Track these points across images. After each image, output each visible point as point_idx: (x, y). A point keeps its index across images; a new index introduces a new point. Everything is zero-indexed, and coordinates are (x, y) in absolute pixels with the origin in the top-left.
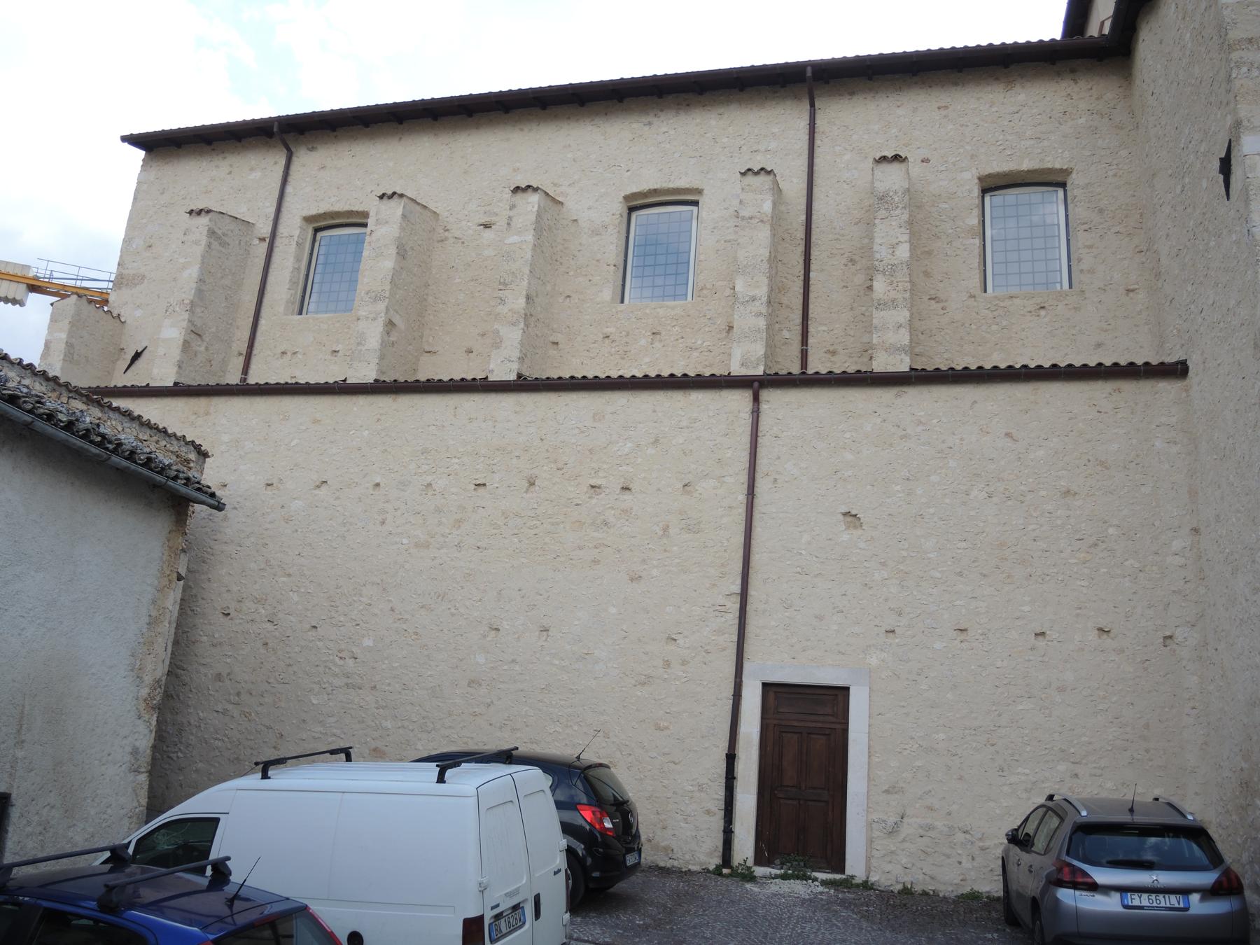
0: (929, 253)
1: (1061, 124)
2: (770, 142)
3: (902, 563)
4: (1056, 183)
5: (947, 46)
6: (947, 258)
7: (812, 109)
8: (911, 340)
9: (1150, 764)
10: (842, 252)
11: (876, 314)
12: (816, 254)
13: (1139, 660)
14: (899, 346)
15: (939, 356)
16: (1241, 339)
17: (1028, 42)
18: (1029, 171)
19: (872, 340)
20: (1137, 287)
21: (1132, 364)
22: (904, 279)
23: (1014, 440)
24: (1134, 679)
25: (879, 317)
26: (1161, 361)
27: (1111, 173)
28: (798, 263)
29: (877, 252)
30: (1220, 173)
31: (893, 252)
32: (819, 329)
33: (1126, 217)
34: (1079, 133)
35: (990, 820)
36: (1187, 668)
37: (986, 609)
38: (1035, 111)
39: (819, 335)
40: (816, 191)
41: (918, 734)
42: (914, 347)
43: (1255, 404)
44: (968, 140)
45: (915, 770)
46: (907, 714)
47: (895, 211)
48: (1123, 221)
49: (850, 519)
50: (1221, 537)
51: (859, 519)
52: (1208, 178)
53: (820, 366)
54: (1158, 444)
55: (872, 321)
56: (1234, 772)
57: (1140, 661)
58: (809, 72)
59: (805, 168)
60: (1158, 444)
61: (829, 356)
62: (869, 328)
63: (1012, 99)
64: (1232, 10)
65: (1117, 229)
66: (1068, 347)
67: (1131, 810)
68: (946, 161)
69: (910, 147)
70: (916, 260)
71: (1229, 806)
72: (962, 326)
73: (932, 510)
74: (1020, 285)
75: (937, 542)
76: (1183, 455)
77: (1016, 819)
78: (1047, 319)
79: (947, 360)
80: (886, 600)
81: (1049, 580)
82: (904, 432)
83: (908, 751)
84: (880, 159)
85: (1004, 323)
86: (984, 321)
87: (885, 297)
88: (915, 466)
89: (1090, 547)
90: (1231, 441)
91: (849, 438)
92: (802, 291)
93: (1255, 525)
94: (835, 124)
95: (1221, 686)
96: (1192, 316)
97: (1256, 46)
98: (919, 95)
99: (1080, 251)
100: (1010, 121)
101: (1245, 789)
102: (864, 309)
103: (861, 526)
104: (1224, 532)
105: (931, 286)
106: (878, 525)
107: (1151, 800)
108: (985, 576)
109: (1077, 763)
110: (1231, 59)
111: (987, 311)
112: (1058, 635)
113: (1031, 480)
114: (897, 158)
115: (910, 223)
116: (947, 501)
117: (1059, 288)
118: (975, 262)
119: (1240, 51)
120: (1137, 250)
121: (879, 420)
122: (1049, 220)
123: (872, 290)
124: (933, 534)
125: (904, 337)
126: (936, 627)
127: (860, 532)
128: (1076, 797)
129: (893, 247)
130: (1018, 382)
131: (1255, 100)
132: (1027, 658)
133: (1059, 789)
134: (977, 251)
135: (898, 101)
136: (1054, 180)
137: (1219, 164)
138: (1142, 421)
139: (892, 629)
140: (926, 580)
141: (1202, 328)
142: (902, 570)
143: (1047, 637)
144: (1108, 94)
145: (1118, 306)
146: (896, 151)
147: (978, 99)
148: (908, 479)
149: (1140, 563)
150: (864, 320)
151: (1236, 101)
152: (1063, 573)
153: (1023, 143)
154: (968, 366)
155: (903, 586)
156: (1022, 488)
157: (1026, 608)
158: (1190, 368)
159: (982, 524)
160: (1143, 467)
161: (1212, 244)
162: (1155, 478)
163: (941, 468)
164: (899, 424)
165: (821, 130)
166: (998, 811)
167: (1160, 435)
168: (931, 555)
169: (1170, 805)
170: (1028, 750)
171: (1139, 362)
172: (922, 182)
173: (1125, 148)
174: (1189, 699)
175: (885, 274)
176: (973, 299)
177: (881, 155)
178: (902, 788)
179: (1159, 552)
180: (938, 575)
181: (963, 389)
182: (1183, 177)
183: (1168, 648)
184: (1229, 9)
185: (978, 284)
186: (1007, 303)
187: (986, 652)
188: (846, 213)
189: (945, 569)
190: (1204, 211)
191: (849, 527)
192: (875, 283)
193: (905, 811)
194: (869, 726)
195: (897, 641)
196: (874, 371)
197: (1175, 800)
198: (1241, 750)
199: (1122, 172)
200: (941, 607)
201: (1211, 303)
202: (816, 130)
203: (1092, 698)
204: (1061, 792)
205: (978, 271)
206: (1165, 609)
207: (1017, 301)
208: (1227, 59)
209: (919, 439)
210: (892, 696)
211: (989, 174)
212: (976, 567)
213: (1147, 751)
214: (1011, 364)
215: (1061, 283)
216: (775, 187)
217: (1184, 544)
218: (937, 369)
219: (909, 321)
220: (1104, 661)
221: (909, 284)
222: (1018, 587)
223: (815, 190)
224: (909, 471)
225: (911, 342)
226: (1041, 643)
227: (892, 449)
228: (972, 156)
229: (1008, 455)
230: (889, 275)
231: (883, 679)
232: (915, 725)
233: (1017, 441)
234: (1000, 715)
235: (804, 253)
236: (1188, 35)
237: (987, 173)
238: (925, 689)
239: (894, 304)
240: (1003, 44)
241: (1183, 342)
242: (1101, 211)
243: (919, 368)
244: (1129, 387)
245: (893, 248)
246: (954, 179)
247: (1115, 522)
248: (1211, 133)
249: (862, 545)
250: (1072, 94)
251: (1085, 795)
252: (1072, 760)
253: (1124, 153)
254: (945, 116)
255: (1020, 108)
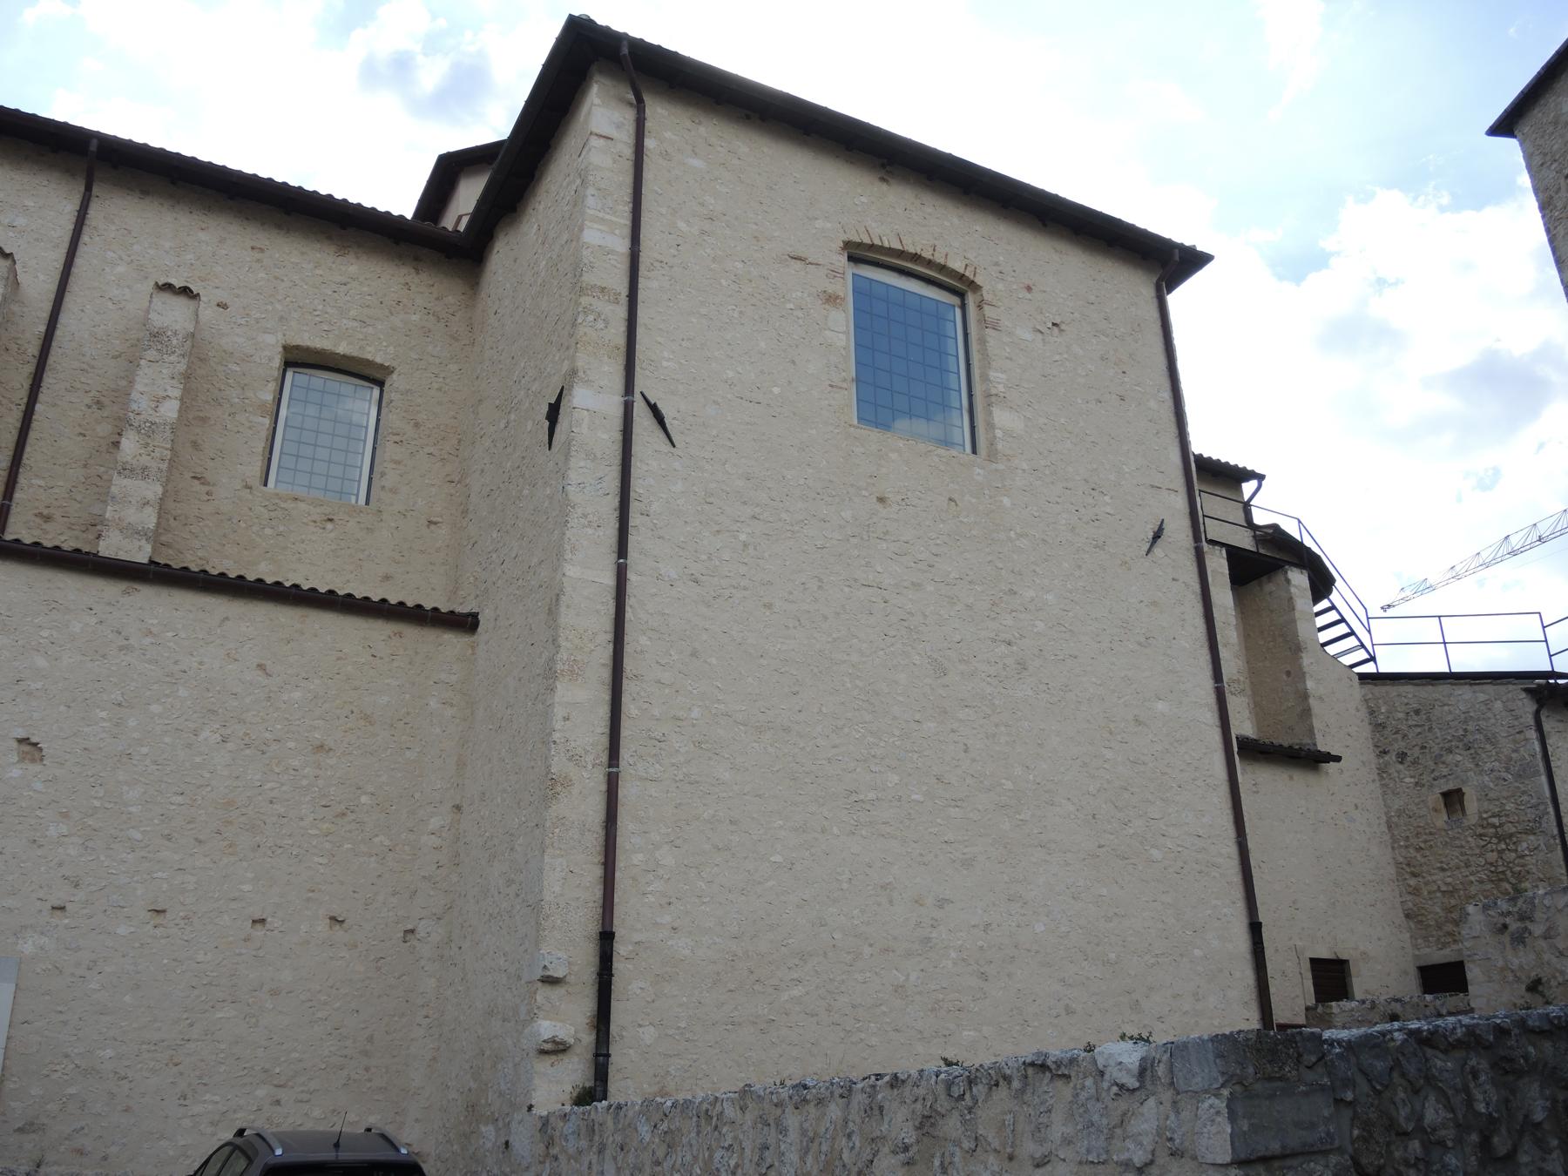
0: (204, 420)
1: (392, 314)
2: (17, 216)
3: (92, 815)
4: (373, 379)
5: (264, 174)
6: (226, 432)
7: (87, 193)
8: (158, 524)
9: (369, 1085)
10: (88, 389)
11: (117, 480)
12: (51, 381)
13: (373, 957)
14: (140, 528)
15: (191, 552)
16: (537, 602)
17: (388, 213)
18: (344, 356)
19: (105, 512)
20: (439, 520)
21: (419, 607)
22: (163, 445)
23: (267, 674)
24: (363, 980)
25: (120, 484)
26: (451, 609)
27: (435, 386)
28: (22, 386)
29: (136, 402)
30: (546, 419)
31: (157, 407)
32: (33, 481)
33: (443, 439)
34: (410, 330)
35: (159, 1165)
36: (426, 969)
37: (196, 886)
38: (365, 289)
39: (31, 490)
40: (68, 299)
41: (76, 1051)
42: (161, 533)
43: (539, 675)
44: (280, 298)
45: (64, 1099)
46: (65, 1023)
47: (170, 355)
48: (438, 442)
49: (27, 748)
50: (483, 818)
51: (41, 749)
52: (534, 421)
53: (24, 532)
54: (433, 704)
55: (109, 487)
56: (462, 1093)
57: (374, 960)
58: (94, 146)
59: (60, 265)
60: (433, 704)
61: (38, 520)
62: (104, 497)
63: (342, 267)
64: (592, 252)
65: (431, 450)
66: (352, 572)
67: (337, 1145)
68: (247, 315)
69: (207, 282)
70: (185, 425)
71: (451, 1134)
72: (229, 520)
73: (145, 750)
74: (326, 490)
75: (145, 793)
76: (458, 720)
77: (194, 1161)
78: (332, 535)
79: (200, 559)
80: (60, 865)
81: (281, 854)
82: (126, 642)
83: (60, 1073)
84: (164, 285)
85: (281, 528)
86: (256, 521)
87: (134, 462)
88: (132, 689)
89: (337, 816)
90: (509, 711)
91: (46, 638)
92: (18, 425)
93: (520, 808)
94: (114, 223)
95: (459, 992)
96: (492, 566)
97: (607, 298)
98: (231, 224)
99: (385, 465)
100: (335, 292)
101: (471, 1113)
102: (102, 469)
103: (42, 760)
104: (487, 813)
105: (198, 461)
106: (66, 761)
107: (363, 1131)
108: (200, 842)
109: (280, 1086)
110: (581, 303)
111: (262, 509)
112: (281, 923)
113: (279, 727)
114: (185, 291)
115: (187, 377)
116: (167, 740)
117: (353, 501)
118: (260, 446)
119: (590, 298)
120: (449, 479)
121: (94, 620)
122: (356, 418)
123: (118, 448)
124: (140, 781)
125: (149, 519)
126: (125, 905)
127: (37, 768)
128: (274, 1130)
129: (159, 401)
130: (284, 604)
131: (595, 353)
132: (237, 951)
133: (254, 1121)
134: (264, 434)
135: (203, 222)
136: (370, 375)
137: (547, 409)
138: (419, 675)
139: (63, 905)
140: (120, 841)
141: (500, 581)
142: (90, 826)
143: (267, 925)
144: (450, 298)
145: (416, 538)
146: (187, 282)
147: (303, 253)
148: (119, 705)
149: (391, 840)
150: (99, 484)
151: (577, 348)
152: (299, 846)
153: (345, 321)
154: (226, 572)
155: (87, 847)
156: (267, 735)
157: (247, 887)
158: (481, 623)
159: (208, 775)
160: (412, 727)
161: (526, 492)
162: (423, 743)
163: (167, 696)
164: (120, 630)
165: (94, 223)
166: (171, 1153)
167: (436, 694)
168: (133, 809)
169: (384, 1136)
170: (221, 1070)
171: (428, 606)
172: (213, 331)
173: (456, 362)
174: (423, 1006)
175: (139, 432)
176: (249, 490)
177: (166, 281)
178: (43, 1125)
179: (415, 829)
180: (138, 836)
181: (214, 600)
182: (509, 413)
183: (408, 944)
184: (590, 250)
185: (258, 474)
186: (289, 505)
187: (187, 941)
188: (102, 340)
189: (148, 829)
190: (524, 455)
191: (24, 758)
192: (124, 441)
193: (43, 1156)
194: (8, 1038)
195: (66, 921)
196: (100, 554)
197: (390, 1130)
198: (472, 1067)
199: (447, 387)
200: (135, 879)
201: (514, 555)
202: (87, 222)
203: (310, 1004)
204: (255, 1122)
205: (261, 458)
206: (411, 898)
207: (302, 506)
208: (576, 301)
209: (144, 655)
210: (47, 998)
211: (298, 346)
212: (192, 829)
213: (367, 1069)
214: (280, 580)
215: (357, 495)
216: (11, 276)
217: (443, 822)
218: (186, 569)
219: (161, 499)
220: (331, 958)
221: (169, 452)
222: (241, 860)
223: (68, 298)
224: (122, 694)
225: (157, 527)
226: (259, 932)
227: (106, 661)
228: (281, 318)
229: (256, 691)
230: (145, 434)
231: (38, 974)
232: (75, 1038)
233: (270, 676)
234: (191, 1025)
235: (32, 376)
236: (544, 263)
237: (294, 344)
238: (95, 989)
239: (144, 473)
240: (345, 201)
241: (478, 593)
242: (417, 425)
243: (162, 562)
244: (412, 634)
245: (158, 401)
246: (253, 339)
247: (370, 789)
248: (545, 374)
249: (39, 786)
250: (410, 284)
251: (285, 1127)
252: (275, 1082)
253: (453, 367)
254: (258, 261)
255: (349, 280)
